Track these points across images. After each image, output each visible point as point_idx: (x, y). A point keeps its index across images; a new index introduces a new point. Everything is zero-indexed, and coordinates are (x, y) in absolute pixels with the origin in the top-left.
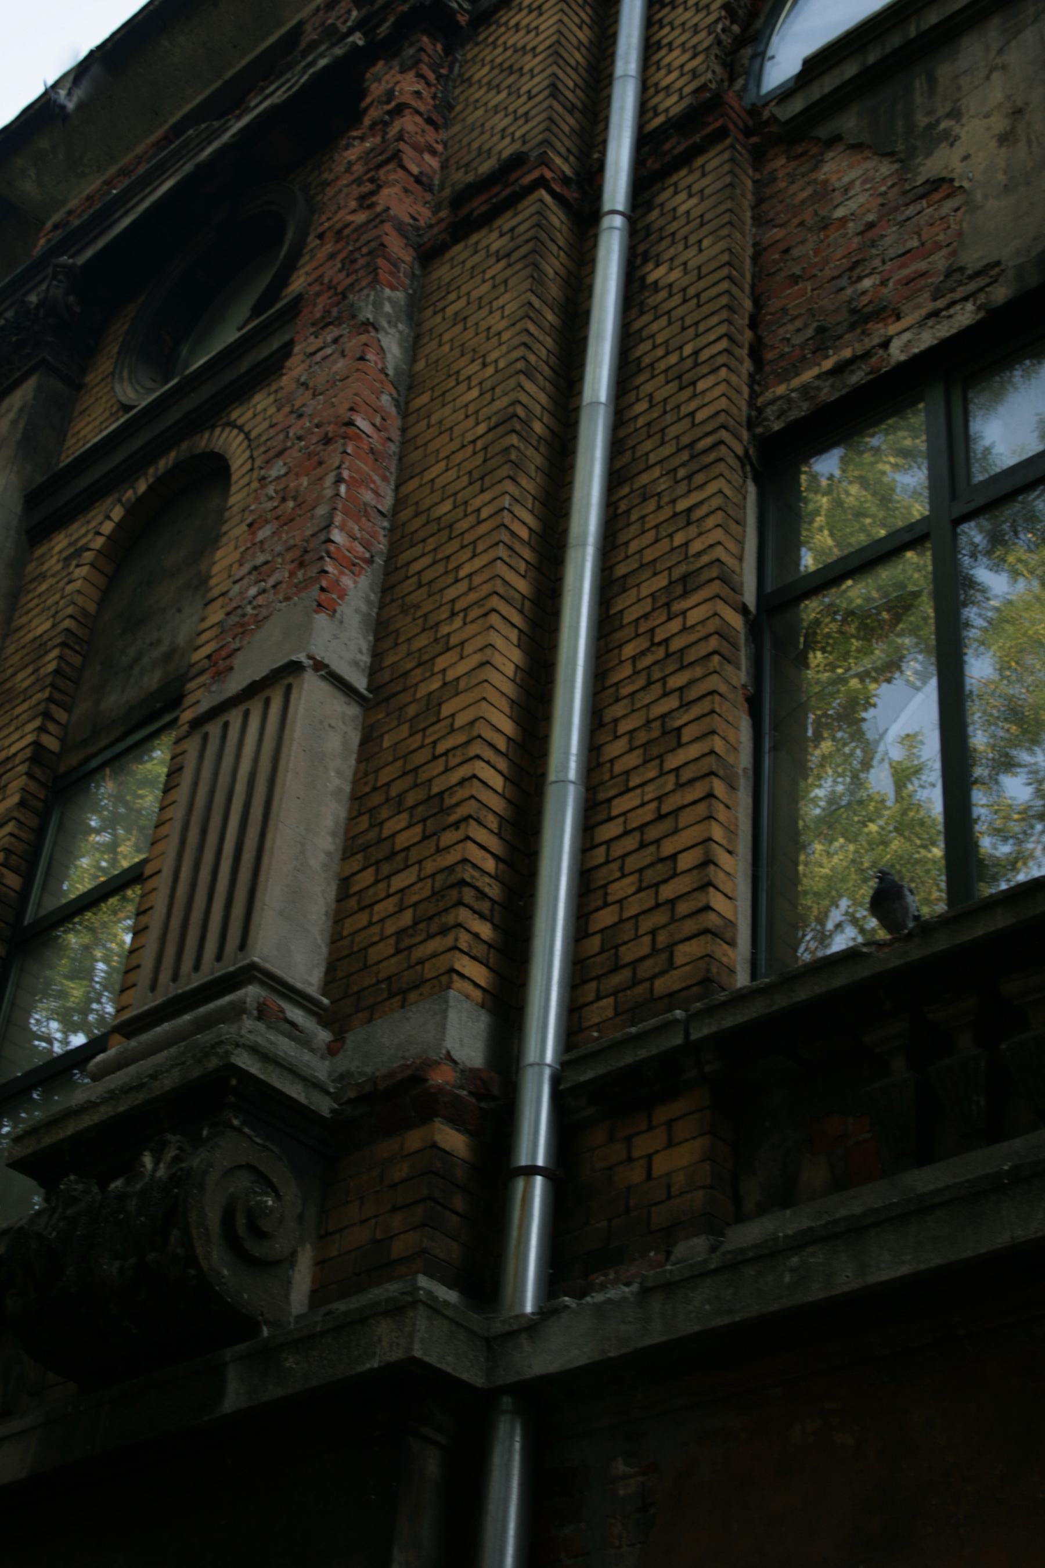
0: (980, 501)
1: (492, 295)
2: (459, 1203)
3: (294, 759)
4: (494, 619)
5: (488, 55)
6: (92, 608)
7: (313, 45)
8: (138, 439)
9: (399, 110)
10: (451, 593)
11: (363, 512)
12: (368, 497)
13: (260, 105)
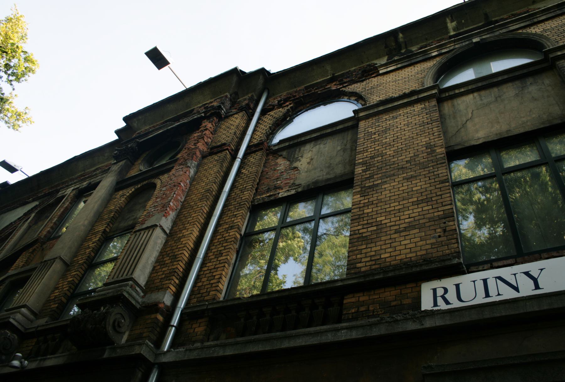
0: (286, 225)
1: (213, 167)
2: (158, 329)
3: (151, 242)
4: (195, 226)
5: (226, 124)
6: (123, 206)
7: (195, 113)
8: (142, 176)
9: (206, 129)
10: (189, 219)
11: (177, 200)
12: (179, 198)
13: (182, 122)
